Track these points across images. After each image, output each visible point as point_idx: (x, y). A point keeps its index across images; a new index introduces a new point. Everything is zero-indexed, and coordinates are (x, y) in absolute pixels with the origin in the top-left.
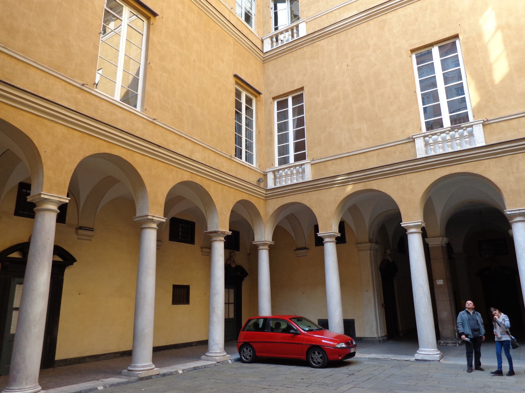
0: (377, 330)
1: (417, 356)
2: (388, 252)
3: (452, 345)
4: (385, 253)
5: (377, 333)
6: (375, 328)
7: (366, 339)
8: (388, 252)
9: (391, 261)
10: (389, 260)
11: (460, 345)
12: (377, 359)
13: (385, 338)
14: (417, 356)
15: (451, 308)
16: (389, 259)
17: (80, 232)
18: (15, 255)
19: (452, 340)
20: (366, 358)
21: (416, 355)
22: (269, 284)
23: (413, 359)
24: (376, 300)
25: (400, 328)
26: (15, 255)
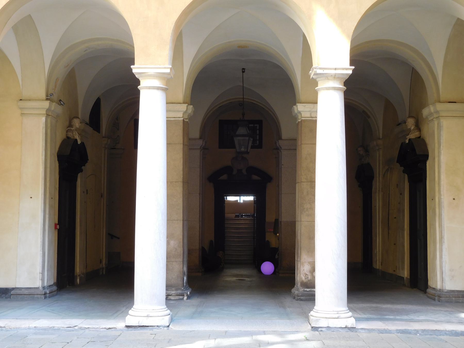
0: (43, 273)
1: (131, 320)
2: (77, 123)
3: (177, 297)
4: (70, 125)
5: (43, 280)
6: (39, 268)
7: (19, 292)
8: (77, 123)
9: (79, 142)
10: (76, 140)
11: (189, 297)
12: (53, 328)
13: (55, 288)
14: (131, 320)
15: (183, 233)
16: (77, 137)
17: (22, 104)
18: (224, 177)
19: (177, 290)
20: (29, 328)
21: (128, 317)
22: (58, 160)
23: (121, 325)
24: (47, 216)
25: (78, 270)
26: (224, 177)
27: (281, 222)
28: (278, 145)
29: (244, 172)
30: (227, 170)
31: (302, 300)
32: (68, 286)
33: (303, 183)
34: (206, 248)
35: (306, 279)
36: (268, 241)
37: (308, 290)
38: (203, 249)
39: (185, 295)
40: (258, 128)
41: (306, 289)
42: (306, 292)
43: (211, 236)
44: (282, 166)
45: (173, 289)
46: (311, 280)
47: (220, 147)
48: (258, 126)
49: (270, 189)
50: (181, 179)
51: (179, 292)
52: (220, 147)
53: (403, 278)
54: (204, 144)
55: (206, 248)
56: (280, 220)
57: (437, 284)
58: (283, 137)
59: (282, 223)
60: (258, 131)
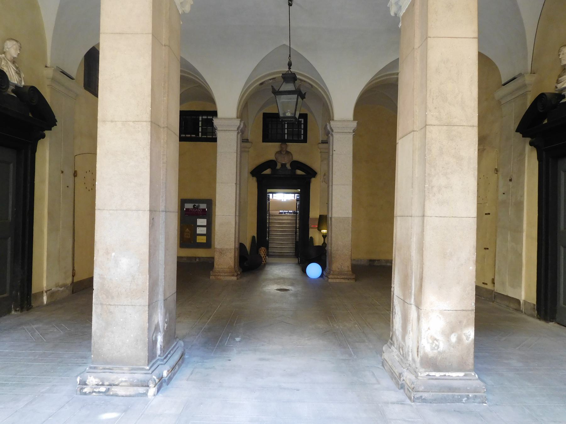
3: (132, 391)
18: (268, 171)
19: (133, 370)
26: (268, 171)
27: (331, 218)
28: (329, 128)
29: (288, 166)
30: (271, 164)
31: (424, 400)
32: (13, 312)
33: (431, 128)
34: (248, 246)
35: (433, 349)
36: (311, 237)
37: (438, 374)
38: (242, 247)
39: (151, 385)
40: (302, 122)
41: (433, 374)
42: (435, 382)
43: (252, 231)
44: (334, 152)
45: (126, 368)
46: (444, 352)
47: (264, 141)
48: (302, 120)
49: (316, 185)
50: (146, 116)
51: (139, 376)
52: (264, 141)
53: (518, 301)
54: (242, 126)
55: (248, 246)
56: (330, 216)
57: (521, 296)
58: (335, 118)
59: (333, 220)
60: (302, 125)
